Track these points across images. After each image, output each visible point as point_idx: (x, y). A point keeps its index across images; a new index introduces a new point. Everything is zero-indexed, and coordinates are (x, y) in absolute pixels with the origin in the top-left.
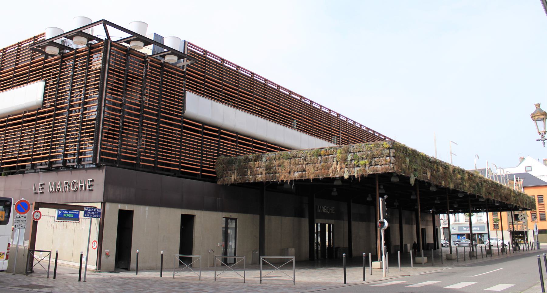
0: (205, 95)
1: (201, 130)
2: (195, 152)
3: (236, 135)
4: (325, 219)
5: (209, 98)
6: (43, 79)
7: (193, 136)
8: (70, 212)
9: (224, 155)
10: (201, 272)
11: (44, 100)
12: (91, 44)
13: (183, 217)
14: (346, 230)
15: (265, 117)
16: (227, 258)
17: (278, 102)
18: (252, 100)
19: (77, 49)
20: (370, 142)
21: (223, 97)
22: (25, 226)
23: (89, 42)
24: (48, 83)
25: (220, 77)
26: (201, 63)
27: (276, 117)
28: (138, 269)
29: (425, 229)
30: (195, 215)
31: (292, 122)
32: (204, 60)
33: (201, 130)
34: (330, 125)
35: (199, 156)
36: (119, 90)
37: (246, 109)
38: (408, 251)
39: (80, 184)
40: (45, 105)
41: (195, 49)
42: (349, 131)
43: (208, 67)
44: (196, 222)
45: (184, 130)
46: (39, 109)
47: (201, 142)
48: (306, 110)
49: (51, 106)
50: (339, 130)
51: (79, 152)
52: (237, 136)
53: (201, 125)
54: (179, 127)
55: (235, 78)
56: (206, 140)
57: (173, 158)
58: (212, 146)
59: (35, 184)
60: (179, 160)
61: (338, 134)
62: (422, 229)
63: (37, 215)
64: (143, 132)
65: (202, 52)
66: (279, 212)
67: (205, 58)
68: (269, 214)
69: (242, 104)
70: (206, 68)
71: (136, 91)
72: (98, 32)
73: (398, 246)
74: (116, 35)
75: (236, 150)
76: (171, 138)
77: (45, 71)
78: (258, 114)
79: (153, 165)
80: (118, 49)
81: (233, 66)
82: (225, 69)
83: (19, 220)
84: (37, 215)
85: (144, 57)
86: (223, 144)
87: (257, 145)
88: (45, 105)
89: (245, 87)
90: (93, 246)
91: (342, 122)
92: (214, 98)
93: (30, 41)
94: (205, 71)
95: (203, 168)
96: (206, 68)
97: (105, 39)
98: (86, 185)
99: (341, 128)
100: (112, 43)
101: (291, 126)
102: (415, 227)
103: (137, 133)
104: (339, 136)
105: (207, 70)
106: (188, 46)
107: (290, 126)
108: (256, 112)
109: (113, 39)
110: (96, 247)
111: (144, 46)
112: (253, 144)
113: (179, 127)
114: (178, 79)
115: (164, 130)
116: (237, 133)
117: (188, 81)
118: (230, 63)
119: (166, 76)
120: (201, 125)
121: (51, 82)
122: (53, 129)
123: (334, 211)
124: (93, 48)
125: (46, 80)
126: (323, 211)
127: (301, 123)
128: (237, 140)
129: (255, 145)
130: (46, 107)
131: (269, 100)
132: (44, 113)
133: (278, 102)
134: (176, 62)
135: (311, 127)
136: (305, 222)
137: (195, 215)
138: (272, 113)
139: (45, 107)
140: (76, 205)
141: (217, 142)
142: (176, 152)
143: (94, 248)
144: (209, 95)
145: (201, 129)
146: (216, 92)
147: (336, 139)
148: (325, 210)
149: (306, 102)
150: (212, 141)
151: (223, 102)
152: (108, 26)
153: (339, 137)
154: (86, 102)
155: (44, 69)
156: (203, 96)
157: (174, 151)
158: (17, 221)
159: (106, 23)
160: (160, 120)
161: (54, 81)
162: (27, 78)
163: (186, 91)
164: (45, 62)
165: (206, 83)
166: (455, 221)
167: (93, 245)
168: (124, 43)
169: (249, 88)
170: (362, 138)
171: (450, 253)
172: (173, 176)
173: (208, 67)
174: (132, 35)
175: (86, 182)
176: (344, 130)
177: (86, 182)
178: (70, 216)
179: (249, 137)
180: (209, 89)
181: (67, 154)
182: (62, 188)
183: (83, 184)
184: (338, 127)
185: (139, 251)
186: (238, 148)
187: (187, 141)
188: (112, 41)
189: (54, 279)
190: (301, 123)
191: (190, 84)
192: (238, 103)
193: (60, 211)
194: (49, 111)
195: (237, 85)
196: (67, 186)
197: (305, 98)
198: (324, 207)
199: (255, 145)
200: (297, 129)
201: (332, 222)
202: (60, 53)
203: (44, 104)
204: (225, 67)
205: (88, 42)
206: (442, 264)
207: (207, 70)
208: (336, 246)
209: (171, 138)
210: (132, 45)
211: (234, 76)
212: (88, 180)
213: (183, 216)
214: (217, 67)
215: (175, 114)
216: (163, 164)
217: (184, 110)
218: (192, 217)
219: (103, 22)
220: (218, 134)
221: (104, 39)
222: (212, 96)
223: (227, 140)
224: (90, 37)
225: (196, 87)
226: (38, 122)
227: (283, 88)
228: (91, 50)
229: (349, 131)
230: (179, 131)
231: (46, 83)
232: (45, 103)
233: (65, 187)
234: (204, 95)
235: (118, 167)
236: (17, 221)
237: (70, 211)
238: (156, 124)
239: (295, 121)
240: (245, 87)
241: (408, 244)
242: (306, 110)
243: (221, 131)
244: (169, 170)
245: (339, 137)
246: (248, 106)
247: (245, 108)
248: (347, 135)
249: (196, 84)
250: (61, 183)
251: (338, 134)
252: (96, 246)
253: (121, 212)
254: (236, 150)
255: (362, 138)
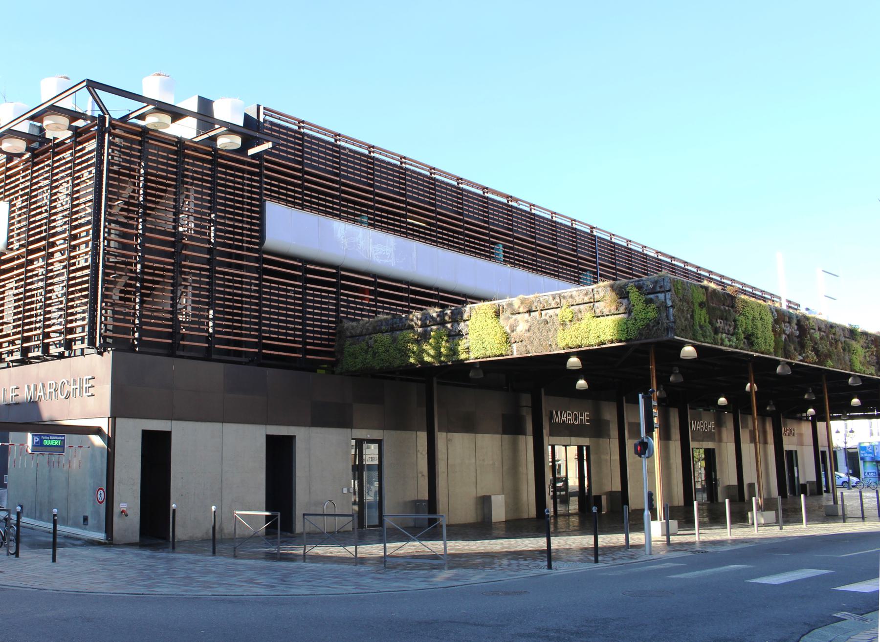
0: (305, 205)
1: (301, 274)
3: (373, 280)
4: (571, 435)
7: (319, 293)
8: (51, 438)
12: (77, 128)
13: (271, 440)
14: (616, 457)
15: (434, 241)
16: (429, 513)
17: (485, 219)
18: (433, 220)
19: (55, 139)
20: (651, 275)
21: (466, 243)
23: (74, 124)
24: (14, 205)
26: (293, 146)
27: (457, 241)
28: (212, 542)
29: (714, 450)
30: (295, 436)
31: (493, 248)
33: (301, 274)
34: (612, 263)
35: (299, 324)
36: (232, 229)
37: (393, 227)
38: (720, 500)
42: (635, 266)
43: (378, 176)
45: (265, 277)
48: (584, 245)
49: (22, 246)
50: (595, 260)
51: (66, 328)
53: (300, 264)
54: (370, 292)
55: (366, 169)
56: (312, 292)
57: (246, 329)
60: (257, 334)
61: (594, 268)
62: (790, 453)
65: (295, 124)
66: (469, 425)
67: (337, 148)
68: (449, 430)
69: (386, 220)
70: (305, 155)
71: (164, 208)
72: (84, 103)
73: (424, 501)
74: (117, 107)
75: (375, 309)
76: (240, 292)
77: (10, 184)
78: (447, 245)
79: (170, 341)
85: (180, 143)
87: (417, 297)
89: (419, 194)
91: (602, 243)
92: (323, 211)
95: (308, 347)
96: (305, 155)
97: (99, 115)
99: (599, 254)
100: (113, 122)
101: (490, 256)
102: (771, 448)
103: (207, 292)
104: (596, 270)
105: (378, 181)
106: (266, 115)
107: (487, 256)
108: (444, 242)
109: (117, 115)
112: (411, 296)
114: (231, 175)
115: (224, 278)
116: (375, 276)
117: (269, 181)
118: (354, 141)
119: (224, 176)
120: (300, 264)
123: (588, 421)
124: (80, 135)
125: (12, 200)
126: (564, 421)
127: (510, 248)
128: (376, 289)
129: (414, 296)
130: (14, 248)
131: (441, 207)
132: (12, 260)
133: (485, 219)
135: (533, 255)
136: (527, 443)
137: (295, 436)
138: (452, 234)
141: (334, 296)
142: (233, 316)
143: (100, 501)
144: (273, 194)
146: (383, 214)
147: (590, 277)
148: (566, 418)
149: (521, 207)
150: (323, 294)
151: (344, 218)
153: (595, 273)
154: (74, 235)
156: (301, 208)
157: (246, 316)
159: (92, 85)
160: (215, 259)
163: (266, 200)
165: (305, 184)
166: (872, 434)
167: (99, 496)
168: (134, 119)
170: (646, 272)
171: (834, 503)
172: (246, 364)
173: (378, 176)
176: (640, 270)
179: (430, 288)
180: (273, 182)
181: (49, 333)
182: (45, 394)
183: (78, 386)
184: (593, 252)
186: (378, 304)
187: (277, 298)
188: (111, 119)
190: (510, 248)
191: (289, 193)
193: (35, 438)
195: (337, 173)
197: (516, 200)
198: (565, 412)
199: (414, 296)
200: (504, 261)
201: (585, 441)
202: (28, 149)
203: (9, 244)
207: (378, 181)
208: (594, 493)
209: (240, 292)
210: (151, 121)
211: (365, 166)
213: (269, 437)
214: (327, 151)
215: (247, 247)
216: (228, 342)
217: (262, 238)
220: (335, 280)
221: (97, 116)
222: (288, 199)
223: (363, 291)
225: (317, 201)
227: (469, 183)
229: (635, 266)
230: (256, 279)
231: (11, 206)
233: (50, 392)
234: (303, 207)
235: (139, 352)
237: (51, 435)
238: (208, 267)
239: (501, 246)
240: (419, 194)
241: (602, 497)
242: (584, 245)
244: (239, 354)
245: (595, 273)
246: (426, 231)
247: (389, 226)
248: (613, 268)
249: (285, 186)
250: (43, 386)
251: (594, 268)
253: (147, 435)
254: (375, 309)
255: (646, 272)
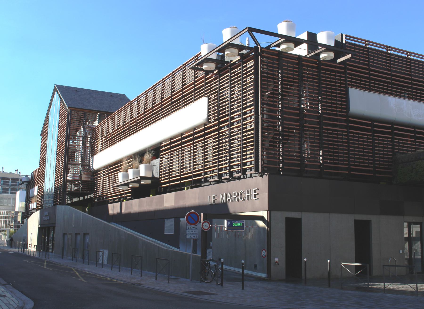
2: (331, 148)
5: (422, 101)
6: (206, 96)
9: (400, 153)
10: (418, 285)
11: (209, 116)
12: (243, 54)
19: (231, 61)
22: (196, 236)
24: (211, 98)
25: (408, 73)
32: (388, 57)
39: (247, 194)
40: (210, 120)
41: (354, 41)
44: (127, 212)
46: (206, 125)
47: (371, 141)
52: (415, 130)
58: (386, 144)
59: (209, 196)
63: (206, 226)
64: (305, 137)
65: (363, 43)
76: (329, 139)
80: (268, 54)
81: (402, 53)
82: (393, 58)
83: (191, 230)
84: (206, 226)
85: (299, 58)
86: (402, 141)
88: (210, 120)
89: (420, 74)
90: (263, 255)
93: (191, 61)
94: (391, 68)
97: (255, 46)
98: (252, 195)
100: (262, 49)
110: (265, 255)
111: (295, 47)
113: (345, 127)
121: (213, 97)
122: (218, 143)
130: (212, 121)
134: (333, 58)
139: (210, 122)
140: (153, 208)
143: (264, 256)
145: (370, 127)
151: (373, 90)
152: (255, 34)
155: (206, 86)
158: (189, 231)
159: (251, 30)
161: (215, 96)
162: (193, 96)
164: (205, 79)
169: (384, 65)
174: (321, 47)
175: (251, 191)
177: (251, 191)
178: (239, 225)
182: (231, 199)
183: (250, 194)
185: (307, 260)
188: (261, 48)
189: (222, 287)
192: (412, 94)
193: (228, 222)
194: (214, 126)
196: (236, 196)
204: (393, 56)
205: (240, 53)
206: (88, 264)
207: (393, 68)
212: (254, 189)
218: (367, 223)
219: (247, 30)
224: (240, 48)
226: (206, 137)
228: (244, 59)
230: (345, 132)
231: (209, 99)
232: (210, 118)
236: (189, 231)
238: (318, 126)
243: (350, 119)
250: (230, 194)
252: (265, 254)
253: (289, 220)
